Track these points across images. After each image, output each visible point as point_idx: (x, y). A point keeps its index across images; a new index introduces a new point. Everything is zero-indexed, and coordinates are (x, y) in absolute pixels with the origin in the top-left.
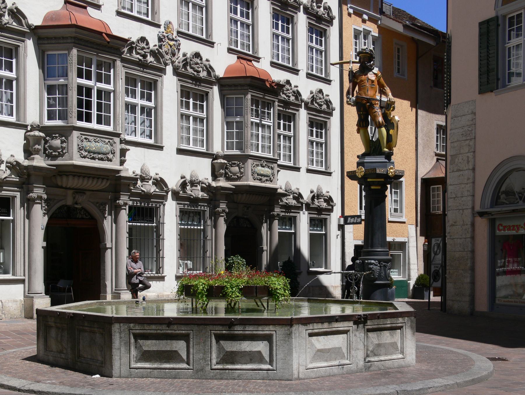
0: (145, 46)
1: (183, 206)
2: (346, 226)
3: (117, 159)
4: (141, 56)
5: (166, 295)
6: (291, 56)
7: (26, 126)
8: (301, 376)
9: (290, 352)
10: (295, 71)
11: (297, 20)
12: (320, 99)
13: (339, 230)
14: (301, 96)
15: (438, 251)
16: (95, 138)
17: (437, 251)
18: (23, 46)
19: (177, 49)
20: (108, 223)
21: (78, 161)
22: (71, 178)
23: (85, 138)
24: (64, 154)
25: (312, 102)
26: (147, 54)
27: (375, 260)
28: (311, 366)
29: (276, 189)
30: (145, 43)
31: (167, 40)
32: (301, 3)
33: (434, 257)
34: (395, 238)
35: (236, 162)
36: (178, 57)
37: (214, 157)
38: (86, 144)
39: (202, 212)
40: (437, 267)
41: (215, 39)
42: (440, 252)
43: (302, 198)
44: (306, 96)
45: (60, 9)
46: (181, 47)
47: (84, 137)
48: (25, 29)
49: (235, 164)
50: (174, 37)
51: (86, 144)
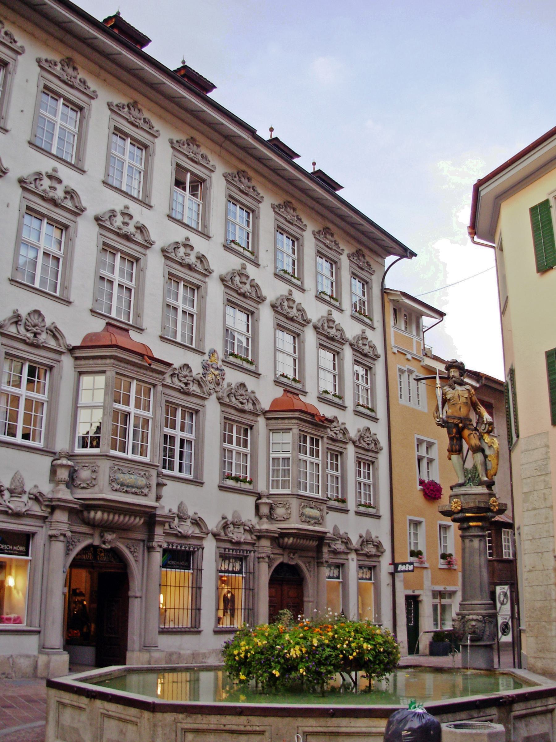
0: (188, 374)
3: (153, 495)
7: (55, 453)
10: (343, 408)
15: (505, 600)
17: (503, 601)
26: (189, 382)
29: (326, 533)
33: (500, 607)
34: (446, 587)
38: (120, 476)
40: (505, 619)
42: (507, 602)
43: (351, 543)
44: (353, 434)
46: (225, 377)
48: (62, 349)
50: (218, 366)
51: (120, 476)
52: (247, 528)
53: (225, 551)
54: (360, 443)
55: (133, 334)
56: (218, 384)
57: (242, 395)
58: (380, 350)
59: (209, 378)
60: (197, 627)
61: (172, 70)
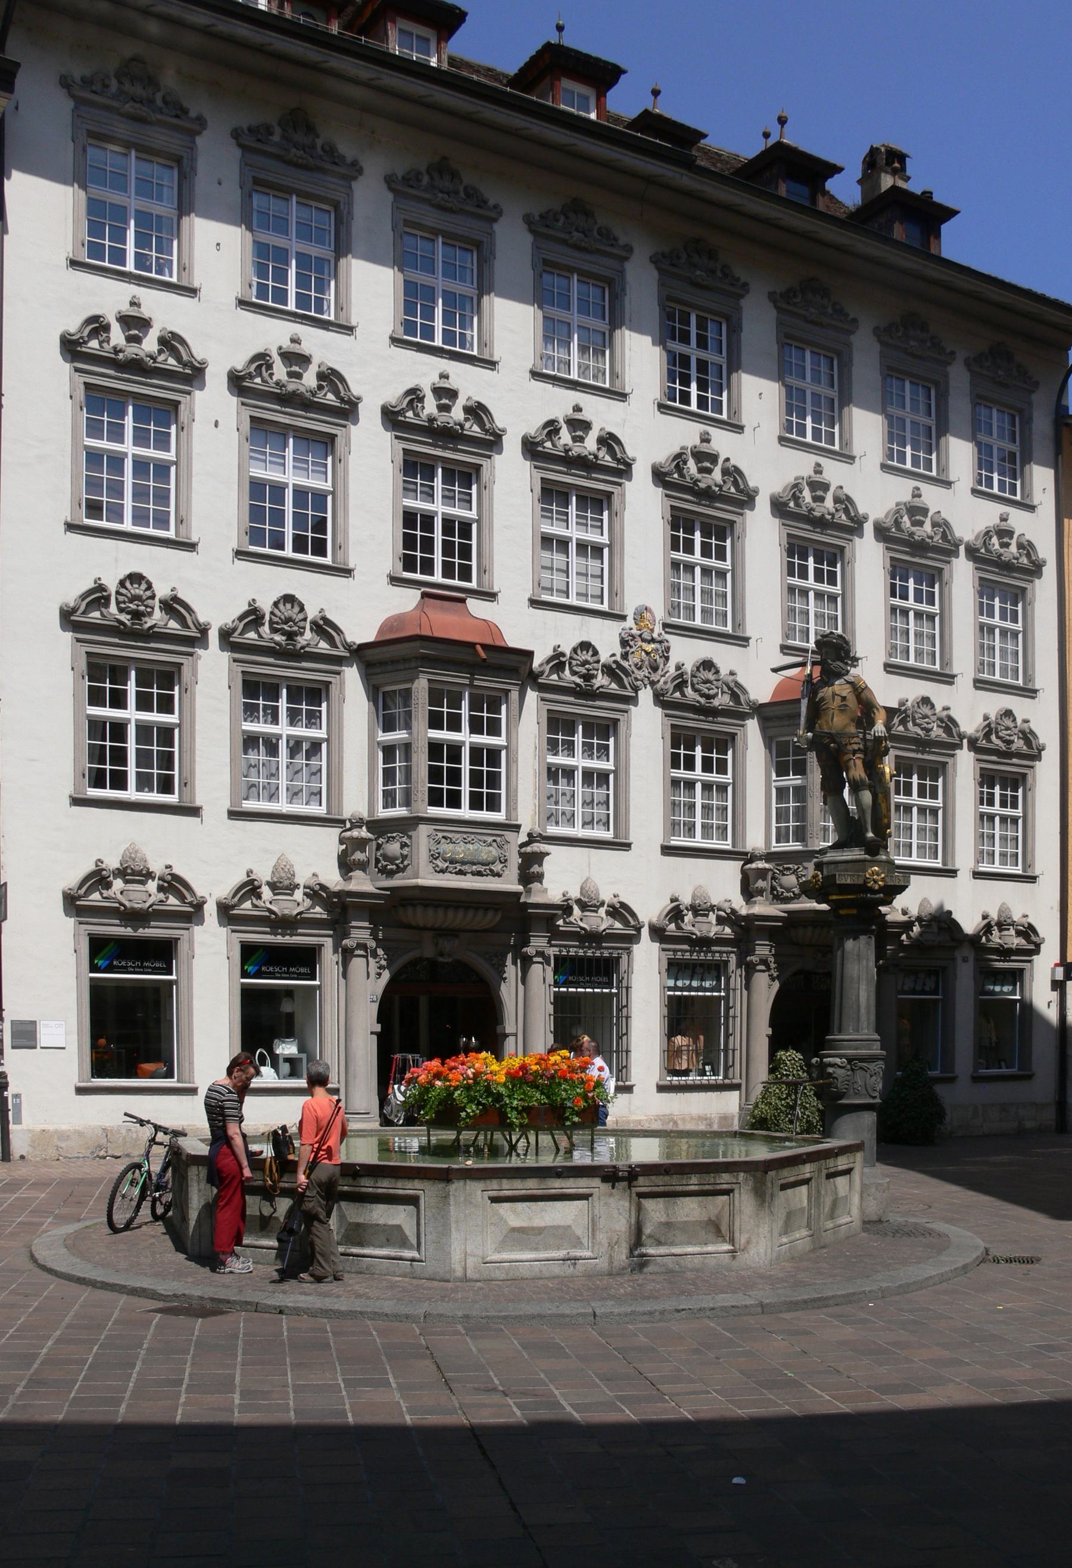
1: (672, 953)
2: (1068, 983)
3: (512, 872)
4: (580, 677)
5: (635, 1121)
6: (937, 649)
7: (343, 822)
8: (470, 1274)
9: (445, 1231)
10: (946, 678)
11: (951, 576)
12: (1007, 729)
13: (1053, 989)
14: (958, 726)
16: (465, 836)
18: (338, 682)
19: (661, 657)
20: (509, 992)
21: (429, 879)
22: (419, 910)
23: (443, 837)
24: (406, 867)
25: (987, 736)
27: (840, 1056)
28: (496, 1257)
30: (590, 653)
31: (640, 643)
32: (958, 542)
35: (791, 866)
36: (666, 673)
37: (748, 858)
38: (446, 848)
39: (722, 965)
41: (751, 630)
44: (969, 724)
45: (412, 608)
47: (440, 835)
48: (342, 652)
49: (789, 869)
52: (943, 925)
53: (560, 951)
54: (989, 741)
55: (475, 606)
56: (655, 669)
57: (925, 717)
58: (1046, 550)
59: (634, 659)
60: (624, 1079)
61: (943, 226)
